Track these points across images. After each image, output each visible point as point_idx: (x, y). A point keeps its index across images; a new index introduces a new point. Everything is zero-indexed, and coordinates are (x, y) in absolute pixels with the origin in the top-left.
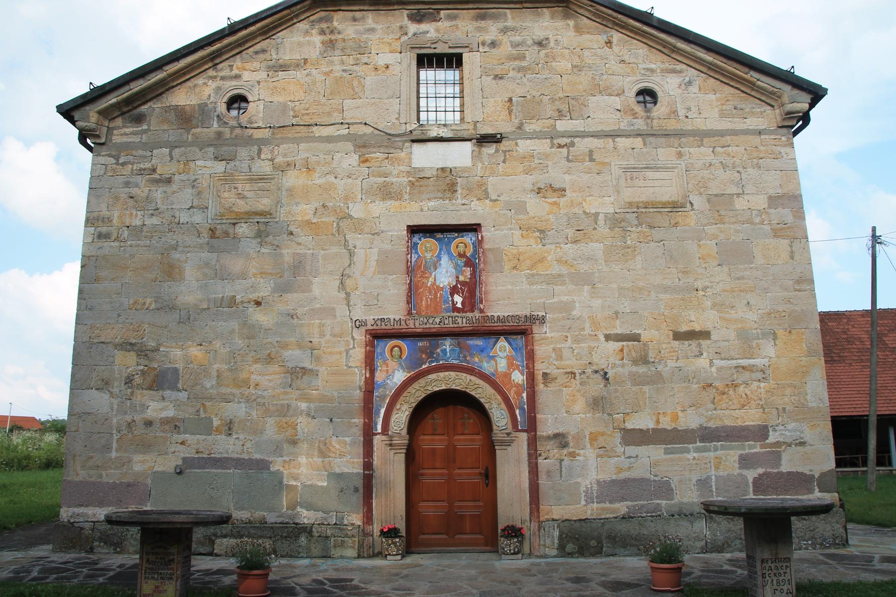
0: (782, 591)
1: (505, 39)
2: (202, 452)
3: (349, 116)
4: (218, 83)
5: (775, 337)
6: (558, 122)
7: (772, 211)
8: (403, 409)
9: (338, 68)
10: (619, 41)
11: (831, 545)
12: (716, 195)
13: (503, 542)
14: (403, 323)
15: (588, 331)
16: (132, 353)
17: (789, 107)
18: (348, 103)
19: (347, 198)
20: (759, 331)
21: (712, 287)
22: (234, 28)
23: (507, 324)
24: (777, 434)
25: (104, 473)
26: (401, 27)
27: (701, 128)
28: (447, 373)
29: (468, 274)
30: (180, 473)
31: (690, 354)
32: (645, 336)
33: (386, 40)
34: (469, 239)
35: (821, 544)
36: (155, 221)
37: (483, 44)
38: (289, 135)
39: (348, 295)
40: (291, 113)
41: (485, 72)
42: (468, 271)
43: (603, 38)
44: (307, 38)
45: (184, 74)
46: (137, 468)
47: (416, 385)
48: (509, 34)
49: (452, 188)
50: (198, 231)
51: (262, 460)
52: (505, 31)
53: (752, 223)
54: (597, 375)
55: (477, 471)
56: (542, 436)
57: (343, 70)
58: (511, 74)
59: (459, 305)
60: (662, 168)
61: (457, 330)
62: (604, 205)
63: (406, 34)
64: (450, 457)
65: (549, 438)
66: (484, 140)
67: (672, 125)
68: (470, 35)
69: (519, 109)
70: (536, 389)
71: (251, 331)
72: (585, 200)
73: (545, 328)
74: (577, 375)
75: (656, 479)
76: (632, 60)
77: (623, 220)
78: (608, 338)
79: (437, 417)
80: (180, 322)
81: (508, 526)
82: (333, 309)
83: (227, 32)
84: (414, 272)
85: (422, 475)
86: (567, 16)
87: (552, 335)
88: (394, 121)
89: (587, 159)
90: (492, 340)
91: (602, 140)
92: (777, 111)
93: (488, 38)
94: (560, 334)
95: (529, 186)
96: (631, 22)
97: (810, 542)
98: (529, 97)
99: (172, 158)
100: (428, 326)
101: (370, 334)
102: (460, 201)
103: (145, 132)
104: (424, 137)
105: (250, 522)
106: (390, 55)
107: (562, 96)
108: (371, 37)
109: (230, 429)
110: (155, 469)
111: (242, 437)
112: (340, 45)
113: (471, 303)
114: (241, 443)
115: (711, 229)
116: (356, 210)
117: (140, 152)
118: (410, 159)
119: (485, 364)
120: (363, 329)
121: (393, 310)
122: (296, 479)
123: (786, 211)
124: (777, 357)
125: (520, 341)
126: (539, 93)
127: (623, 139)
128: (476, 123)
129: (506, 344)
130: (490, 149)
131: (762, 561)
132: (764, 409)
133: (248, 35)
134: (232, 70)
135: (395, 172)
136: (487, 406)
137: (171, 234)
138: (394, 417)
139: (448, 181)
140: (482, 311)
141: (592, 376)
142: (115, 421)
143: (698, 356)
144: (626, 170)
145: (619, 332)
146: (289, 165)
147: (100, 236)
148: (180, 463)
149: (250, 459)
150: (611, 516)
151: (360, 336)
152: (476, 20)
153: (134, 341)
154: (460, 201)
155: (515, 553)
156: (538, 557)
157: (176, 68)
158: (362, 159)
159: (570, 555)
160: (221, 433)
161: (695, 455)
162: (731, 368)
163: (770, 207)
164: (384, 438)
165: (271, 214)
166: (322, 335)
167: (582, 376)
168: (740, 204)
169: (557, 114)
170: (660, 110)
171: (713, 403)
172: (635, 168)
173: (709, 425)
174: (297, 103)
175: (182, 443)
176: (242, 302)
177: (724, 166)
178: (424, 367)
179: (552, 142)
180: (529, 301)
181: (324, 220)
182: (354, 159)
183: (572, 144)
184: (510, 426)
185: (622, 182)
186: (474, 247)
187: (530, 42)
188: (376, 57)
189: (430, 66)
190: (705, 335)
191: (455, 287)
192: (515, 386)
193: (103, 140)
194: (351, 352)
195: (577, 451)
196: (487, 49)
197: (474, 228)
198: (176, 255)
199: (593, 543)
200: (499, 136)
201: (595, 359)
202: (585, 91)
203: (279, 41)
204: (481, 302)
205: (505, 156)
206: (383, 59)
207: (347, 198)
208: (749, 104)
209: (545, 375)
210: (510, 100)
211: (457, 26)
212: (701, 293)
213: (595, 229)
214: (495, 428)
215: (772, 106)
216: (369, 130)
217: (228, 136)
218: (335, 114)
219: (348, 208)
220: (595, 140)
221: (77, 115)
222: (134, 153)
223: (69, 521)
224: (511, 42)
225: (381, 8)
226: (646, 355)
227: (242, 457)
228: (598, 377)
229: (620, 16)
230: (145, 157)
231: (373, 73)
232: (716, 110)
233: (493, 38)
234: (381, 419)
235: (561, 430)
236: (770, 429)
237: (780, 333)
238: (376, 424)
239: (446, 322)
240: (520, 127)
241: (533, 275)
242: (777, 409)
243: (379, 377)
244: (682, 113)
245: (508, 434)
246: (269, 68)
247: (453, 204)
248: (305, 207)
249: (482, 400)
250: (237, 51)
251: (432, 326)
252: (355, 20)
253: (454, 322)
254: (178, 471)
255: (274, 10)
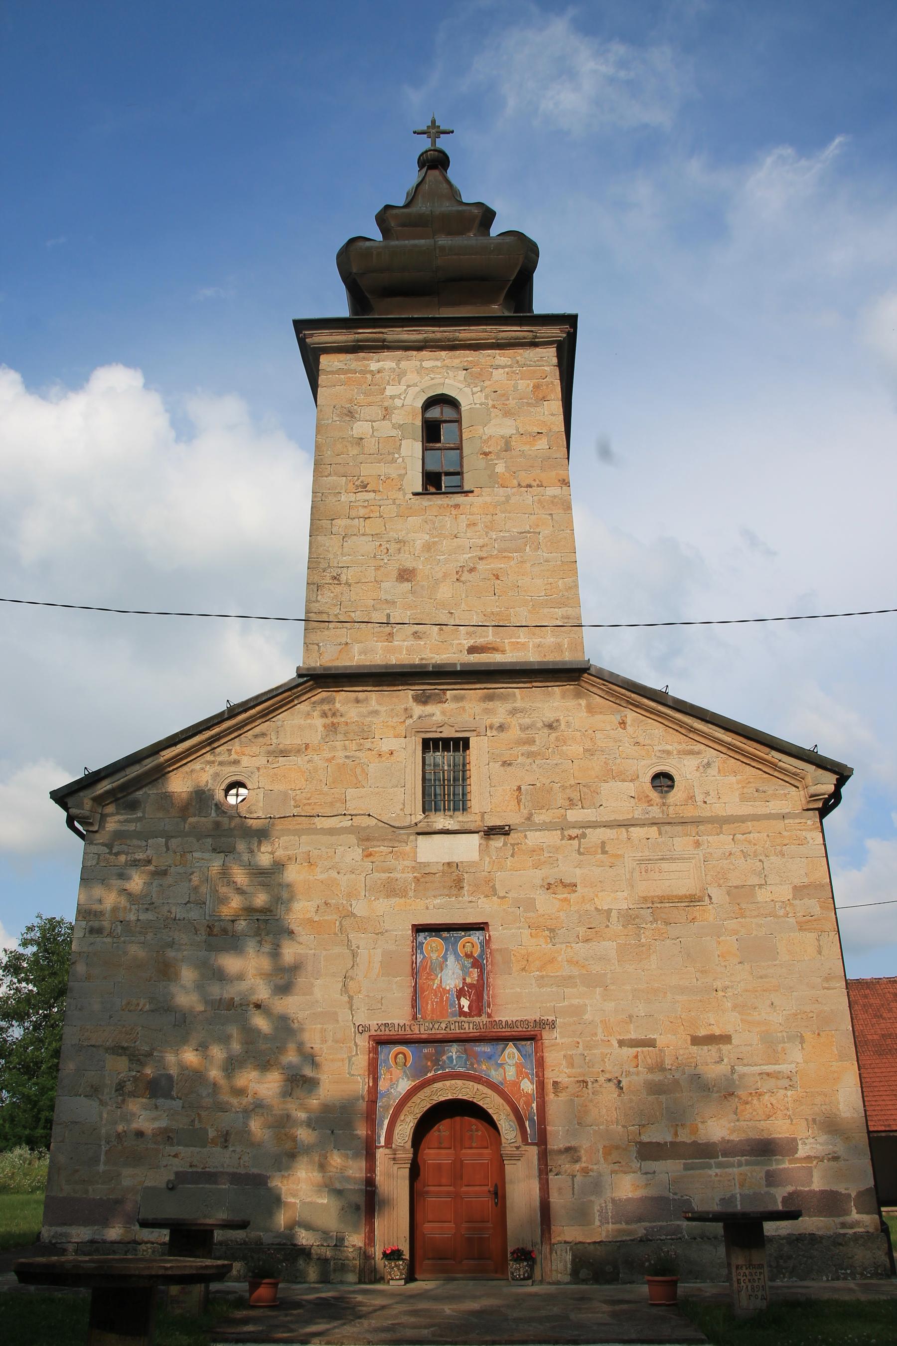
0: (756, 1297)
1: (514, 722)
2: (196, 1166)
3: (352, 808)
4: (216, 768)
5: (802, 1041)
6: (569, 812)
7: (797, 902)
8: (408, 1120)
9: (341, 754)
10: (634, 720)
11: (872, 1275)
12: (736, 887)
13: (513, 1266)
14: (408, 1028)
15: (600, 1036)
16: (124, 1058)
17: (813, 790)
18: (351, 792)
19: (349, 896)
20: (785, 1034)
21: (732, 987)
22: (233, 711)
23: (516, 1029)
24: (808, 1147)
25: (90, 1189)
26: (406, 709)
27: (720, 814)
28: (453, 1082)
29: (476, 975)
30: (172, 1189)
31: (709, 1061)
32: (661, 1041)
33: (390, 723)
34: (476, 937)
35: (862, 1274)
36: (150, 916)
37: (491, 728)
38: (290, 827)
39: (351, 998)
40: (292, 803)
41: (493, 758)
42: (475, 973)
43: (617, 718)
44: (309, 721)
45: (182, 759)
46: (126, 1182)
47: (421, 1095)
48: (518, 715)
49: (458, 884)
50: (195, 928)
51: (259, 1175)
52: (513, 712)
53: (775, 916)
54: (611, 1084)
55: (486, 1188)
56: (553, 1150)
57: (346, 757)
58: (521, 760)
59: (466, 1009)
60: (678, 859)
61: (464, 1036)
62: (618, 900)
63: (411, 717)
64: (457, 1172)
65: (560, 1152)
66: (491, 832)
67: (689, 812)
68: (477, 718)
69: (529, 798)
70: (546, 1099)
71: (250, 1035)
72: (597, 896)
73: (556, 1034)
74: (590, 1083)
75: (676, 1197)
76: (647, 742)
77: (637, 917)
78: (621, 1043)
79: (443, 1129)
80: (175, 1025)
81: (518, 1249)
82: (336, 1013)
83: (226, 716)
84: (419, 974)
85: (427, 1192)
86: (578, 695)
87: (563, 1041)
88: (399, 812)
89: (600, 851)
90: (501, 1046)
91: (615, 831)
92: (802, 793)
93: (496, 721)
94: (570, 1040)
95: (538, 882)
96: (645, 701)
97: (849, 1271)
98: (538, 785)
99: (168, 849)
100: (433, 1032)
101: (374, 1040)
102: (466, 898)
103: (140, 819)
104: (429, 830)
105: (245, 1243)
106: (394, 740)
107: (573, 783)
108: (375, 720)
109: (226, 1141)
110: (146, 1184)
111: (238, 1149)
112: (342, 729)
113: (478, 1008)
114: (237, 1156)
115: (731, 924)
116: (360, 908)
117: (135, 842)
118: (415, 853)
119: (493, 1073)
120: (366, 1035)
121: (398, 1016)
122: (294, 1196)
123: (813, 902)
124: (806, 1062)
125: (529, 1046)
126: (549, 781)
127: (638, 829)
128: (483, 814)
129: (515, 1051)
130: (498, 842)
131: (737, 1267)
132: (792, 1121)
133: (248, 719)
134: (230, 755)
135: (400, 868)
136: (495, 1117)
137: (167, 930)
138: (398, 1129)
139: (454, 877)
140: (489, 1016)
141: (605, 1085)
142: (103, 1131)
143: (718, 1062)
144: (641, 862)
145: (633, 1037)
146: (290, 859)
147: (92, 931)
148: (172, 1177)
149: (247, 1175)
150: (628, 1238)
151: (363, 1042)
152: (484, 701)
153: (126, 1045)
154: (466, 898)
155: (524, 1279)
156: (549, 1283)
157: (174, 753)
158: (365, 853)
159: (584, 1281)
160: (217, 1145)
161: (717, 1171)
162: (754, 1075)
163: (794, 898)
164: (387, 1151)
165: (271, 911)
166: (324, 1041)
167: (595, 1085)
168: (762, 896)
169: (568, 803)
170: (676, 795)
171: (735, 1113)
172: (650, 860)
173: (732, 1138)
174: (298, 792)
175: (176, 1156)
176: (241, 1005)
177: (745, 855)
178: (429, 1075)
179: (562, 834)
180: (538, 1005)
181: (326, 918)
182: (357, 853)
183: (584, 835)
184: (519, 1139)
185: (636, 874)
186: (482, 946)
187: (540, 725)
188: (380, 742)
189: (436, 749)
190: (725, 1039)
191: (462, 989)
192: (525, 1096)
193: (95, 828)
194: (354, 1059)
195: (590, 1167)
196: (495, 733)
197: (481, 927)
198: (171, 954)
199: (609, 1268)
200: (507, 828)
201: (608, 1067)
202: (597, 777)
203: (280, 723)
204: (489, 1006)
205: (514, 849)
206: (385, 746)
207: (349, 896)
208: (773, 786)
209: (555, 1083)
210: (519, 788)
211: (463, 708)
212: (720, 993)
213: (607, 926)
214: (503, 1140)
215: (798, 788)
216: (373, 822)
217: (226, 827)
218: (338, 805)
219: (351, 905)
220: (608, 830)
221: (70, 801)
222: (128, 842)
223: (50, 1242)
224: (520, 725)
225: (385, 688)
226: (663, 1062)
227: (238, 1171)
228: (612, 1086)
229: (633, 695)
230: (140, 847)
231: (377, 760)
232: (737, 793)
233: (501, 720)
234: (384, 1131)
235: (573, 1143)
236: (800, 1142)
237: (808, 1035)
238: (379, 1137)
239: (453, 1027)
240: (529, 818)
241: (542, 977)
242: (807, 1119)
243: (383, 1085)
244: (699, 798)
245: (518, 1148)
246: (270, 753)
247: (460, 902)
248: (307, 904)
249: (490, 1111)
250: (236, 734)
251: (438, 1032)
252: (357, 701)
253: (460, 1028)
254: (170, 1186)
255: (275, 693)
